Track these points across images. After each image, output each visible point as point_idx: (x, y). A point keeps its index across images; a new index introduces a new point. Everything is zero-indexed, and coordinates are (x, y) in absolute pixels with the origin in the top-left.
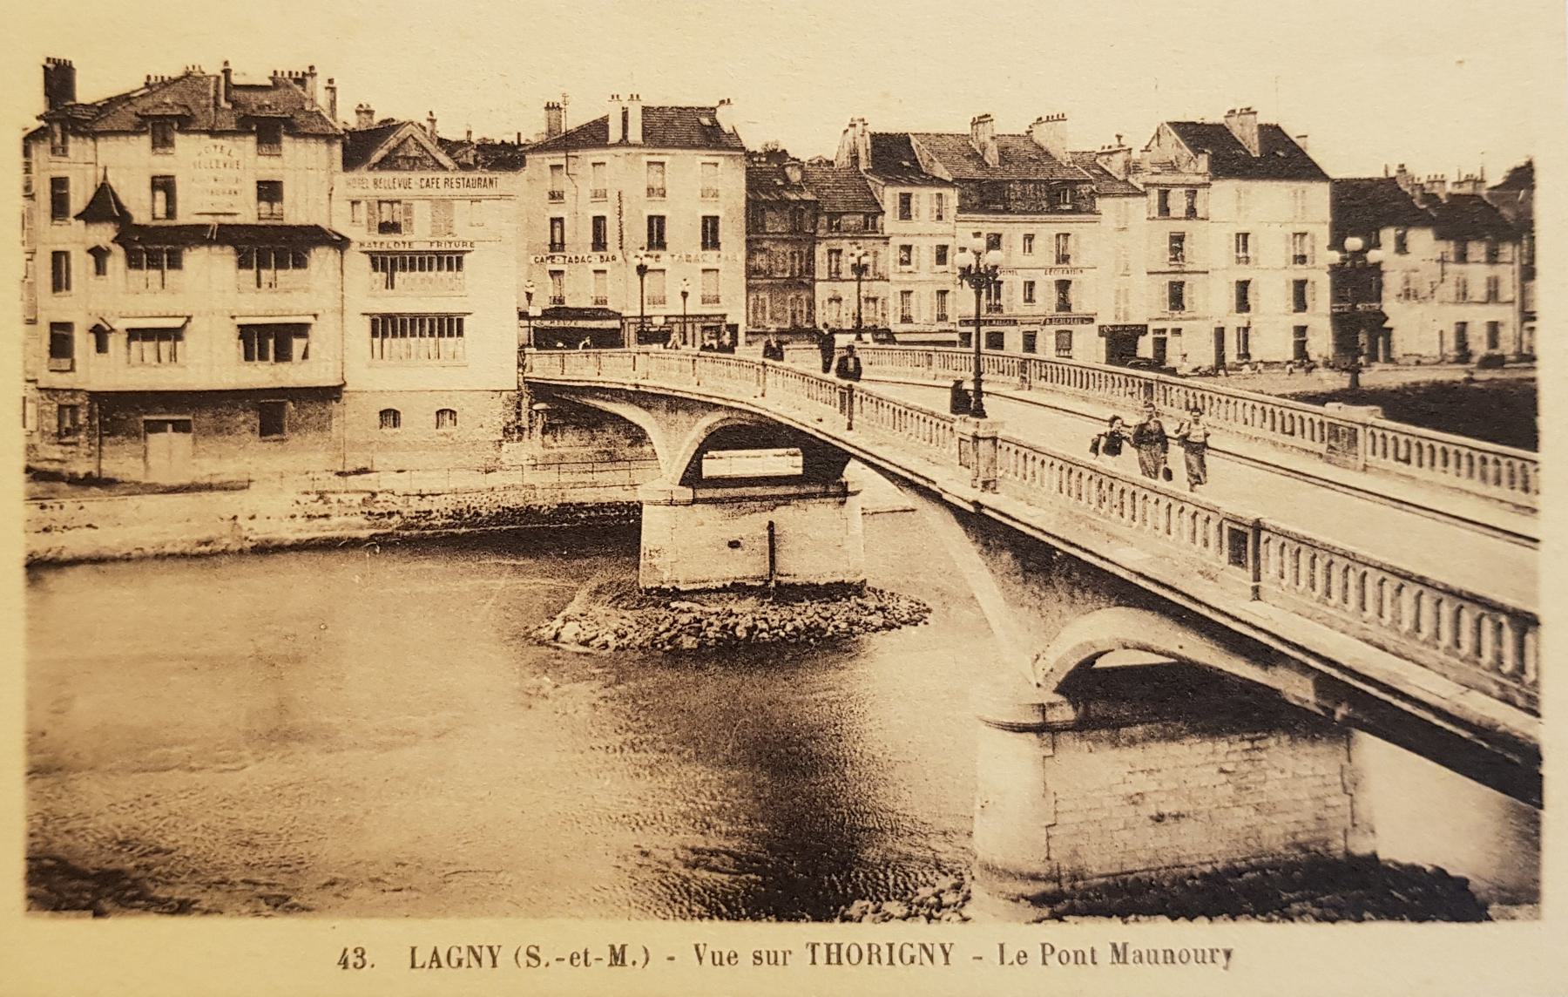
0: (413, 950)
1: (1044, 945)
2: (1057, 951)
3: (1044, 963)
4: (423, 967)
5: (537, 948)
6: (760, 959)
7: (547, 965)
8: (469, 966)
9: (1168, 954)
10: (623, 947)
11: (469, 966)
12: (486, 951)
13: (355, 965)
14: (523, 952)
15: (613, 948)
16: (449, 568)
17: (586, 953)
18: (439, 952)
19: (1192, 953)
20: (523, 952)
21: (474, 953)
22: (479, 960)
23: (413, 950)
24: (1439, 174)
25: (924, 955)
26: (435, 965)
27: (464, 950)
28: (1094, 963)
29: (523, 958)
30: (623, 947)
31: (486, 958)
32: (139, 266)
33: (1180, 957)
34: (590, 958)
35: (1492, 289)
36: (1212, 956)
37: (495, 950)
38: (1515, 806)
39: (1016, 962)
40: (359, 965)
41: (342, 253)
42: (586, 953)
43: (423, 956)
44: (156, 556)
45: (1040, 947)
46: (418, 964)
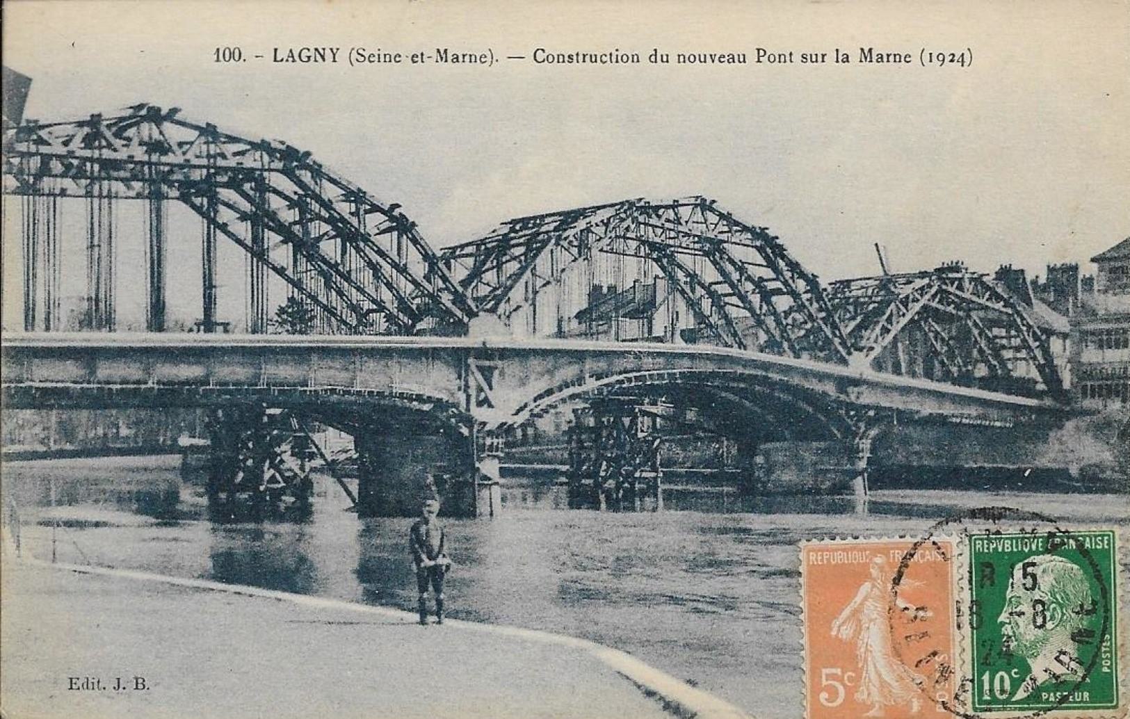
0: (276, 50)
2: (768, 54)
4: (282, 60)
6: (806, 59)
8: (316, 61)
10: (870, 50)
12: (328, 52)
13: (417, 57)
14: (354, 52)
15: (438, 51)
17: (422, 54)
18: (294, 52)
21: (319, 52)
22: (323, 58)
23: (276, 50)
24: (116, 327)
25: (318, 55)
26: (291, 59)
27: (312, 50)
28: (791, 61)
29: (354, 54)
31: (328, 55)
32: (573, 508)
33: (689, 58)
36: (823, 58)
37: (335, 51)
39: (410, 58)
40: (604, 57)
42: (422, 54)
44: (166, 470)
46: (278, 59)
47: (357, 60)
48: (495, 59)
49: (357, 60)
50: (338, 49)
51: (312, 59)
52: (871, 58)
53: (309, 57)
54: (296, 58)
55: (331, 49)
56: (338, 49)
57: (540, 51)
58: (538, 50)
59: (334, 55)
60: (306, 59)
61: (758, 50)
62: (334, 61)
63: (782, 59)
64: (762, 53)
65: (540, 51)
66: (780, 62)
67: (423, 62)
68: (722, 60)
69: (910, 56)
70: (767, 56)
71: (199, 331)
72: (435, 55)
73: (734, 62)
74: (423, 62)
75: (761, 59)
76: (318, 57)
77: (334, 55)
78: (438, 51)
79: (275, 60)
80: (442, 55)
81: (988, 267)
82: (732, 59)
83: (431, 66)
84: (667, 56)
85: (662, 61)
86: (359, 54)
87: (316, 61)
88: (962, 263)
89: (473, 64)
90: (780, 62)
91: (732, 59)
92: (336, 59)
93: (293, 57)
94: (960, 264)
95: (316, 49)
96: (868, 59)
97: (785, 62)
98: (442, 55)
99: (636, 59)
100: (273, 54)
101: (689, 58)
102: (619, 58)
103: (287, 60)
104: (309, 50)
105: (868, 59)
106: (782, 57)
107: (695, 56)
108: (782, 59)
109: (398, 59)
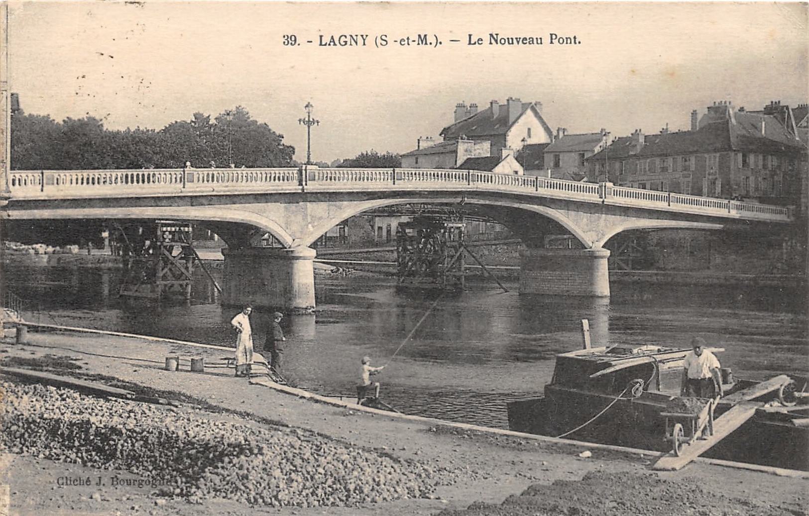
1: (551, 35)
2: (558, 37)
3: (552, 43)
4: (325, 45)
5: (386, 36)
7: (299, 45)
9: (511, 42)
10: (425, 36)
11: (351, 45)
14: (379, 39)
15: (419, 36)
16: (424, 436)
17: (408, 39)
19: (507, 40)
20: (379, 39)
21: (494, 38)
26: (332, 44)
29: (379, 41)
30: (425, 36)
33: (505, 41)
34: (410, 41)
35: (545, 126)
38: (679, 450)
39: (399, 42)
41: (298, 258)
42: (408, 39)
43: (326, 40)
45: (550, 36)
46: (323, 43)
47: (381, 44)
48: (439, 42)
49: (381, 44)
50: (367, 36)
51: (349, 43)
52: (426, 42)
53: (346, 42)
54: (337, 42)
55: (362, 36)
56: (367, 36)
57: (343, 37)
58: (342, 36)
59: (364, 40)
60: (344, 43)
61: (551, 35)
62: (364, 44)
63: (569, 41)
64: (554, 37)
65: (343, 37)
66: (567, 43)
67: (408, 44)
68: (525, 42)
69: (482, 40)
70: (558, 39)
71: (725, 103)
72: (416, 38)
73: (533, 43)
74: (408, 44)
75: (553, 41)
76: (353, 42)
77: (364, 40)
78: (419, 36)
79: (321, 45)
80: (494, 38)
81: (757, 102)
82: (532, 41)
83: (486, 48)
84: (541, 39)
85: (537, 43)
86: (385, 41)
87: (351, 45)
88: (730, 103)
89: (569, 44)
90: (567, 43)
91: (532, 41)
92: (366, 43)
93: (334, 42)
94: (728, 103)
95: (351, 36)
96: (424, 42)
97: (571, 43)
98: (494, 38)
99: (540, 41)
100: (468, 39)
101: (505, 41)
102: (565, 41)
103: (329, 45)
104: (346, 36)
105: (424, 42)
106: (569, 40)
107: (501, 43)
108: (569, 41)
109: (480, 42)
